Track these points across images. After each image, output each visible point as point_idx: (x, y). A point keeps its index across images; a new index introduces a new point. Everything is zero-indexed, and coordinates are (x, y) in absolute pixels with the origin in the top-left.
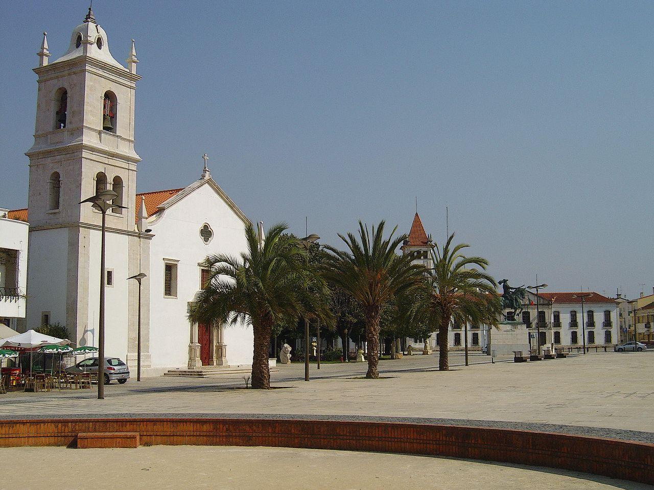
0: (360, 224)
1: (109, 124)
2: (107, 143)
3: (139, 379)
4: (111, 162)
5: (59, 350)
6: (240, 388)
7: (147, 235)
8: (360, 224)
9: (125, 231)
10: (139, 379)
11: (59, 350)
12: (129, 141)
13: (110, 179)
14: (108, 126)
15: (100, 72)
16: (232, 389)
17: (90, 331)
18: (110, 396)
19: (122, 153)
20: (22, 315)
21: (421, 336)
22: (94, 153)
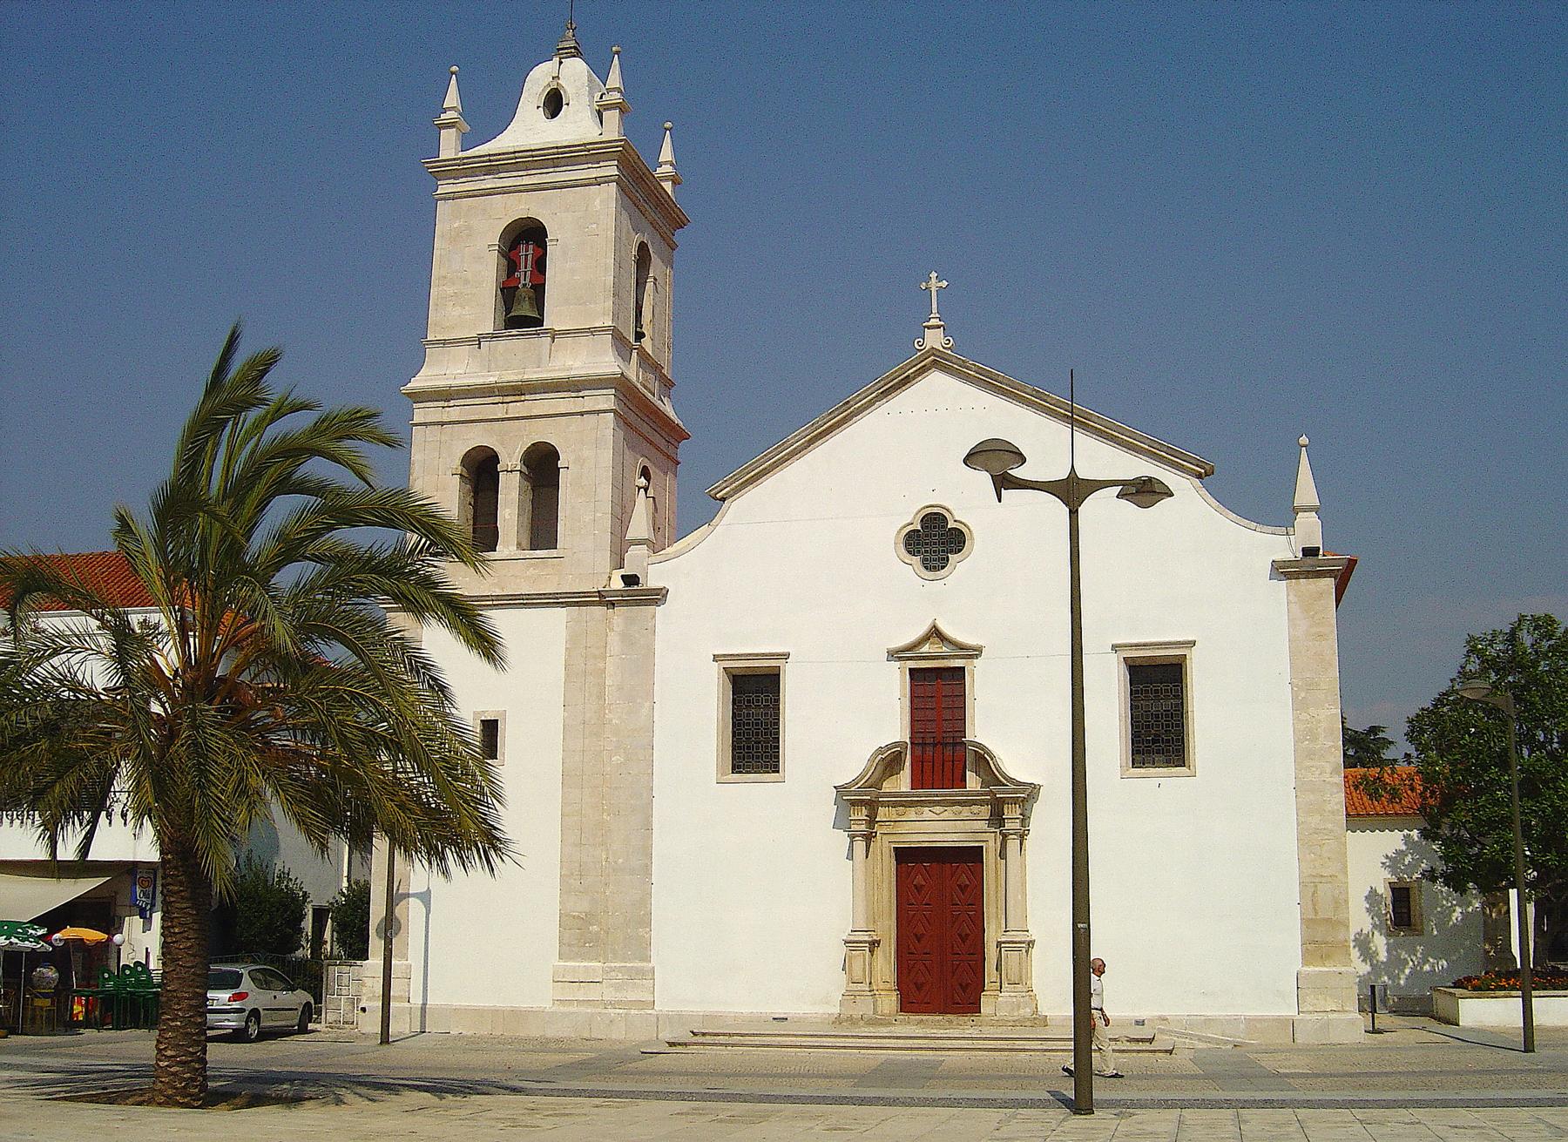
0: (233, 340)
1: (521, 304)
2: (520, 359)
3: (385, 1038)
4: (516, 409)
5: (14, 940)
6: (391, 1088)
7: (637, 593)
8: (233, 340)
9: (555, 595)
10: (385, 1038)
11: (14, 940)
12: (592, 331)
13: (511, 460)
14: (523, 313)
15: (489, 182)
16: (439, 1088)
17: (414, 895)
18: (1111, 1104)
19: (553, 375)
20: (153, 855)
21: (1446, 858)
22: (452, 403)
